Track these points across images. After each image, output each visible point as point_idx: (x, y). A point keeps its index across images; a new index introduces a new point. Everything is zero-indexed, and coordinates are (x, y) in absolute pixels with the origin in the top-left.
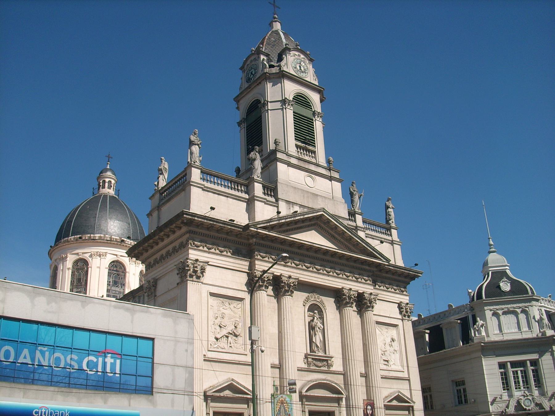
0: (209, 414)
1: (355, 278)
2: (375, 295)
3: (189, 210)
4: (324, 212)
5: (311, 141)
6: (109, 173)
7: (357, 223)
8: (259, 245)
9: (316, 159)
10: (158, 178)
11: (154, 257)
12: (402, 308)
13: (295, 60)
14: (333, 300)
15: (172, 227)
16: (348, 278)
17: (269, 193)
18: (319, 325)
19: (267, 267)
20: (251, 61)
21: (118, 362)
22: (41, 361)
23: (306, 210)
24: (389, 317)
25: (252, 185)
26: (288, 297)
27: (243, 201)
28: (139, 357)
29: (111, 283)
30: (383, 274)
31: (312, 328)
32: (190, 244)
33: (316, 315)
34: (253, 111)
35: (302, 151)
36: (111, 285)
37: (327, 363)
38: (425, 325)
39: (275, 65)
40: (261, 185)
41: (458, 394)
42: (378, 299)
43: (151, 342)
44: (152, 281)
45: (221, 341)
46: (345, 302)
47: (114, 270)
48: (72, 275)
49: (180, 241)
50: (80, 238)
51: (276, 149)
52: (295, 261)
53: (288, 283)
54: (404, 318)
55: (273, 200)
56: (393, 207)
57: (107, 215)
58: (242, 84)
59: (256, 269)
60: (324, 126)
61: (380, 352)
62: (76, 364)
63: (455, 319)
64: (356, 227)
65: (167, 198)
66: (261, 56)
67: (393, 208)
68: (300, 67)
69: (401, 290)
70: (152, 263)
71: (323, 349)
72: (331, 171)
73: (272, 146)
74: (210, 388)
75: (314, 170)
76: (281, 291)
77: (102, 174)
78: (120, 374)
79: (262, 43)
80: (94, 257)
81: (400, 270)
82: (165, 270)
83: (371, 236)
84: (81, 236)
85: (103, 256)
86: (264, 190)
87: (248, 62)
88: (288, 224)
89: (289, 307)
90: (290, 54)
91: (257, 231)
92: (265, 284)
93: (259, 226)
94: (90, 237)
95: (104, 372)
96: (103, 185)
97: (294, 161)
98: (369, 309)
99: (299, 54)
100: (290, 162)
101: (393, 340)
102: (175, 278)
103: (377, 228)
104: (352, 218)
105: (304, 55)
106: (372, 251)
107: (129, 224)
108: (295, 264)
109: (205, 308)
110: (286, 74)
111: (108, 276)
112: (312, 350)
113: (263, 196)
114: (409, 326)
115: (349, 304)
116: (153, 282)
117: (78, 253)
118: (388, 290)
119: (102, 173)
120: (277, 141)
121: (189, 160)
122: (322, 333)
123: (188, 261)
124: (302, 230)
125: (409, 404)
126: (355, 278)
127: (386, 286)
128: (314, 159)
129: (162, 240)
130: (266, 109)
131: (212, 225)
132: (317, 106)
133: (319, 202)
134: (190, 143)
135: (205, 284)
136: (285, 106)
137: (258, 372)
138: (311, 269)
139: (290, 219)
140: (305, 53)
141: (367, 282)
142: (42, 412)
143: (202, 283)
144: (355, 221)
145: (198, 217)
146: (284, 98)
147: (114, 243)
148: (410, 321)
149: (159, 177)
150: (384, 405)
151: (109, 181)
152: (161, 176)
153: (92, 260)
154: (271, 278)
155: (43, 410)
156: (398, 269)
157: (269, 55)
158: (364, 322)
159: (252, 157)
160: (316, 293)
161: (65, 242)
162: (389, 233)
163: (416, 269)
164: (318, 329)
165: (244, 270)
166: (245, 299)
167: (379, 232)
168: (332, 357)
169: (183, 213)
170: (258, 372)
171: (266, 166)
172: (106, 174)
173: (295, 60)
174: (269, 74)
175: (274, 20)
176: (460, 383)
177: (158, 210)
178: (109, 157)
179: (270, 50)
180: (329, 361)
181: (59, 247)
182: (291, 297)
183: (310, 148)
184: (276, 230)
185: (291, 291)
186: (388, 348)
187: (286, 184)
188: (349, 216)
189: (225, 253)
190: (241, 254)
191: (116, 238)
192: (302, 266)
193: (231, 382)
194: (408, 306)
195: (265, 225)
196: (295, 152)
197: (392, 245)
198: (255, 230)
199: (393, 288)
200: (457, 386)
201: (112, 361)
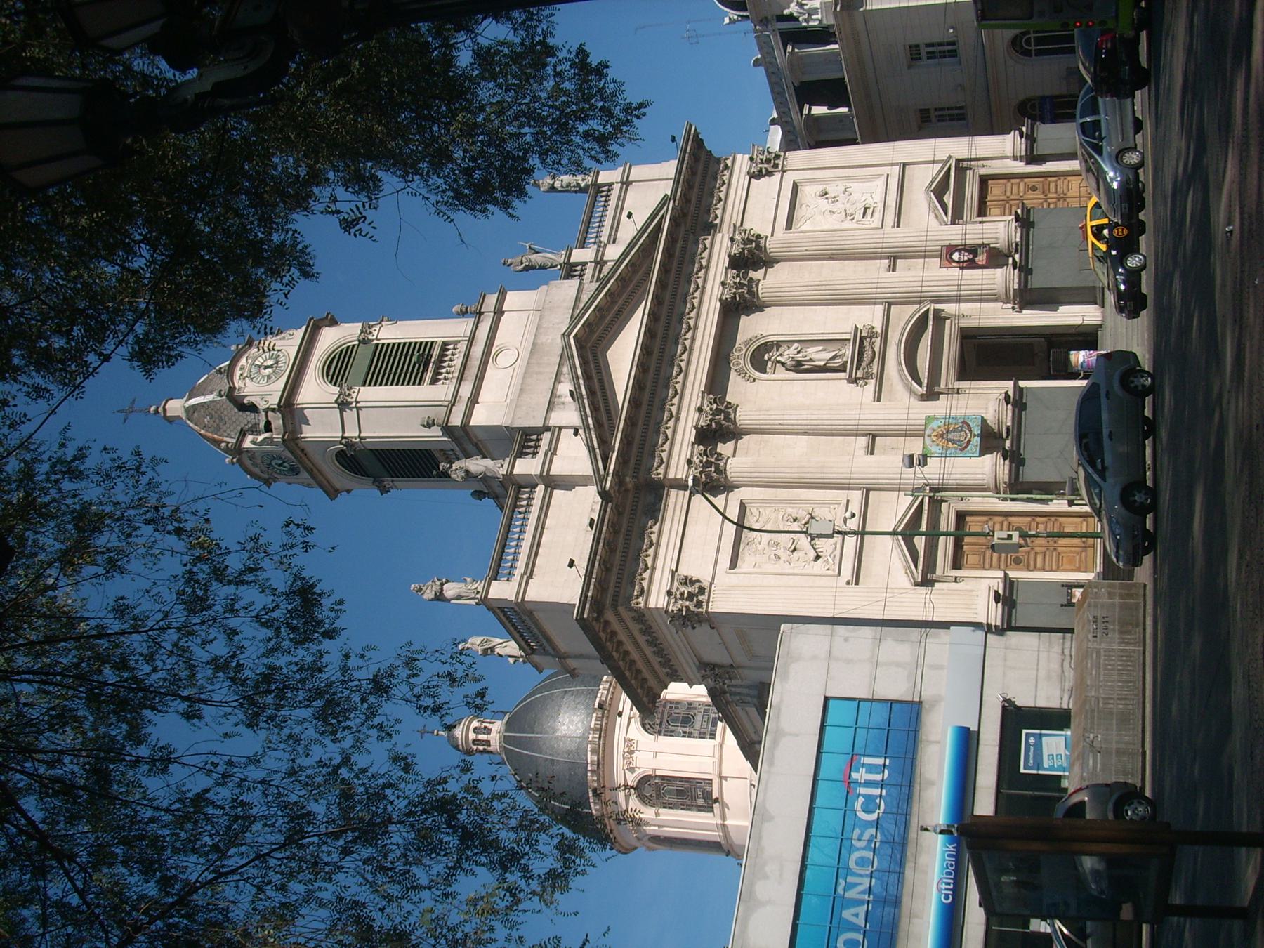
2: (734, 232)
4: (569, 335)
8: (637, 469)
9: (459, 341)
11: (657, 667)
12: (760, 171)
14: (743, 319)
17: (532, 444)
18: (792, 351)
20: (255, 465)
21: (868, 760)
23: (566, 369)
24: (778, 201)
26: (738, 414)
29: (687, 730)
31: (798, 367)
36: (692, 730)
37: (865, 338)
41: (935, 58)
49: (631, 624)
55: (546, 436)
60: (385, 318)
63: (781, 57)
65: (544, 641)
71: (839, 345)
73: (436, 433)
79: (217, 443)
86: (527, 454)
87: (256, 470)
88: (595, 409)
93: (602, 472)
94: (592, 771)
97: (466, 390)
98: (762, 245)
101: (824, 194)
102: (701, 635)
105: (241, 356)
106: (646, 235)
112: (842, 369)
113: (541, 456)
114: (796, 158)
118: (723, 198)
121: (473, 602)
124: (605, 379)
126: (699, 271)
128: (459, 345)
135: (713, 578)
139: (587, 406)
141: (708, 246)
142: (946, 889)
143: (712, 583)
144: (584, 264)
145: (588, 591)
147: (606, 724)
150: (953, 223)
152: (497, 650)
154: (701, 447)
155: (944, 886)
157: (242, 429)
162: (606, 188)
163: (681, 140)
164: (800, 355)
168: (856, 328)
169: (580, 620)
171: (476, 445)
174: (285, 433)
176: (914, 53)
177: (564, 658)
183: (436, 352)
186: (838, 207)
191: (594, 719)
197: (631, 182)
198: (609, 478)
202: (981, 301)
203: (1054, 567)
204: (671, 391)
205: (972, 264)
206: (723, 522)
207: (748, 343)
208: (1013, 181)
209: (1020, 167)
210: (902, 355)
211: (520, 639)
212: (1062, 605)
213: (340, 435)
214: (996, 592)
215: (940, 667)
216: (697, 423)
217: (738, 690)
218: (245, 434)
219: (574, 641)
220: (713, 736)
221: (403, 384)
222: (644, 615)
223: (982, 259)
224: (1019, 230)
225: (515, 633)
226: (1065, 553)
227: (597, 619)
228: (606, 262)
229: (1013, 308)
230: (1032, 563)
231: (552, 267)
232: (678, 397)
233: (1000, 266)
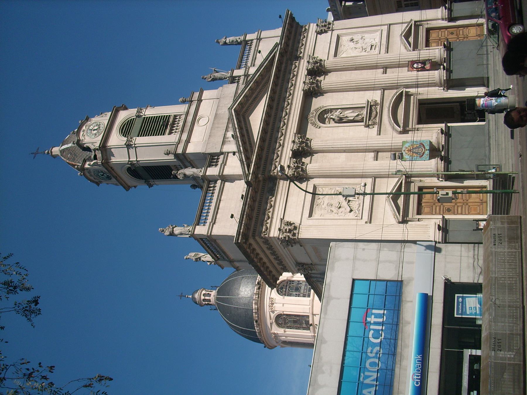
0: (419, 219)
2: (310, 58)
3: (234, 236)
5: (164, 120)
6: (196, 296)
7: (241, 75)
11: (276, 265)
13: (88, 134)
14: (314, 99)
15: (249, 252)
16: (294, 84)
17: (215, 161)
18: (337, 113)
19: (284, 164)
20: (91, 176)
21: (374, 311)
22: (373, 379)
23: (230, 125)
24: (330, 44)
25: (208, 177)
26: (312, 144)
27: (224, 186)
28: (369, 293)
29: (298, 293)
30: (289, 49)
31: (340, 120)
32: (265, 235)
33: (329, 117)
34: (138, 174)
35: (175, 128)
36: (299, 293)
37: (372, 106)
38: (337, 5)
39: (94, 154)
40: (208, 168)
42: (313, 55)
43: (356, 281)
44: (298, 267)
45: (352, 207)
46: (316, 88)
47: (286, 290)
48: (290, 328)
50: (256, 322)
51: (174, 154)
52: (279, 137)
53: (299, 144)
54: (331, 28)
55: (222, 157)
56: (224, 38)
57: (235, 298)
58: (113, 184)
60: (149, 106)
61: (364, 53)
62: (375, 348)
64: (245, 75)
65: (222, 254)
66: (86, 167)
67: (226, 38)
69: (304, 32)
71: (360, 110)
72: (192, 100)
73: (171, 157)
74: (396, 218)
75: (192, 117)
76: (307, 150)
77: (198, 302)
78: (384, 310)
79: (74, 166)
80: (274, 309)
81: (285, 33)
82: (288, 257)
83: (254, 61)
84: (255, 321)
85: (272, 301)
86: (213, 165)
87: (92, 178)
88: (244, 143)
89: (321, 142)
90: (82, 140)
91: (252, 174)
92: (300, 165)
93: (247, 172)
94: (255, 313)
95: (383, 324)
96: (208, 301)
97: (184, 137)
98: (323, 64)
99: (82, 131)
100: (186, 141)
101: (352, 40)
102: (296, 249)
103: (246, 54)
104: (236, 80)
105: (83, 125)
106: (267, 61)
107: (243, 277)
108: (281, 136)
109: (323, 222)
110: (102, 144)
111: (291, 296)
112: (361, 121)
113: (219, 166)
115: (318, 84)
116: (299, 267)
117: (270, 323)
118: (304, 44)
119: (197, 302)
120: (166, 153)
122: (345, 110)
123: (280, 238)
125: (413, 25)
127: (300, 46)
128: (182, 116)
129: (261, 259)
130: (136, 162)
131: (247, 216)
132: (131, 113)
133: (223, 112)
135: (301, 222)
136: (133, 144)
137: (381, 173)
138: (286, 121)
140: (80, 126)
141: (297, 66)
142: (417, 379)
143: (300, 224)
144: (239, 77)
145: (240, 229)
146: (125, 146)
147: (261, 291)
148: (334, 22)
149: (202, 260)
150: (414, 50)
151: (203, 296)
152: (202, 259)
153: (276, 311)
154: (295, 159)
155: (415, 377)
156: (285, 34)
157: (84, 159)
158: (335, 69)
159: (183, 177)
160: (308, 116)
161: (261, 336)
162: (250, 42)
163: (284, 17)
164: (342, 115)
165: (288, 185)
166: (314, 184)
167: (249, 52)
168: (368, 101)
169: (237, 243)
170: (381, 173)
171: (190, 162)
172: (197, 298)
173: (88, 134)
174: (103, 160)
175: (50, 154)
177: (233, 262)
178: (181, 296)
179: (80, 159)
180: (371, 104)
181: (265, 340)
182: (312, 141)
183: (171, 120)
185: (306, 140)
186: (359, 46)
187: (207, 145)
188: (234, 83)
189: (272, 203)
190: (273, 188)
191: (256, 289)
192: (283, 130)
193: (390, 199)
194: (319, 24)
195: (246, 166)
196: (175, 135)
197: (261, 39)
198: (250, 175)
199: (302, 39)
201: (373, 316)
202: (428, 86)
203: (467, 213)
204: (280, 133)
205: (423, 69)
206: (305, 195)
207: (317, 110)
208: (442, 30)
209: (445, 23)
210: (390, 113)
211: (212, 253)
212: (474, 230)
213: (128, 160)
214: (439, 225)
215: (412, 263)
216: (293, 148)
217: (315, 276)
218: (86, 161)
219: (235, 254)
220: (309, 296)
221: (156, 135)
222: (268, 241)
223: (428, 66)
224: (445, 52)
225: (209, 250)
226: (472, 206)
227: (245, 243)
228: (249, 75)
229: (444, 89)
230: (456, 211)
231: (225, 78)
232: (283, 136)
233: (437, 70)
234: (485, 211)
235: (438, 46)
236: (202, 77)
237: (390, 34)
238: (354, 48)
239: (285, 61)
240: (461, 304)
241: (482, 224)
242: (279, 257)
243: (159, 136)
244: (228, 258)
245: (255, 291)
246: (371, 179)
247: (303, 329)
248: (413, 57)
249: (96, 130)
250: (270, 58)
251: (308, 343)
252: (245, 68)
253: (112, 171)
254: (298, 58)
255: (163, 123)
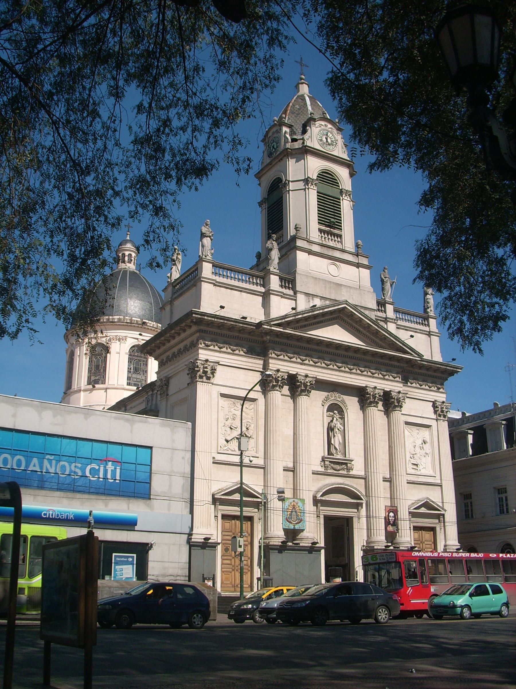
1: (382, 375)
2: (404, 394)
3: (200, 309)
4: (346, 304)
5: (336, 223)
6: (129, 246)
8: (274, 342)
9: (342, 244)
10: (171, 269)
12: (437, 407)
17: (287, 285)
18: (339, 425)
20: (273, 133)
21: (118, 471)
23: (328, 303)
24: (421, 417)
27: (258, 295)
29: (132, 370)
31: (330, 429)
35: (326, 236)
36: (132, 372)
37: (347, 466)
39: (299, 138)
40: (278, 277)
41: (500, 502)
43: (150, 450)
47: (136, 356)
48: (89, 361)
49: (190, 339)
55: (291, 292)
59: (270, 368)
60: (354, 203)
61: (408, 455)
63: (500, 418)
65: (180, 292)
67: (432, 294)
68: (327, 139)
70: (165, 360)
71: (343, 451)
79: (285, 112)
86: (281, 282)
88: (306, 319)
89: (305, 408)
90: (315, 125)
92: (279, 384)
93: (272, 323)
94: (109, 319)
97: (316, 248)
98: (397, 409)
99: (326, 123)
102: (185, 378)
106: (401, 345)
112: (330, 453)
113: (280, 290)
114: (444, 426)
118: (422, 387)
122: (342, 434)
125: (439, 512)
128: (340, 244)
134: (201, 235)
139: (308, 314)
140: (332, 121)
141: (396, 379)
142: (49, 514)
143: (212, 384)
144: (385, 312)
145: (208, 316)
147: (135, 326)
150: (410, 513)
151: (129, 254)
152: (174, 267)
154: (286, 377)
155: (51, 513)
157: (292, 126)
162: (426, 323)
163: (453, 364)
164: (337, 430)
168: (352, 461)
169: (191, 313)
171: (286, 254)
174: (291, 150)
176: (502, 491)
177: (170, 304)
179: (293, 120)
182: (307, 397)
183: (336, 231)
184: (292, 326)
185: (308, 390)
186: (418, 450)
191: (137, 319)
194: (445, 404)
195: (280, 321)
197: (430, 337)
198: (269, 327)
200: (499, 494)
202: (368, 529)
203: (223, 570)
205: (387, 522)
206: (247, 389)
207: (343, 402)
208: (433, 545)
210: (337, 486)
211: (180, 279)
213: (290, 180)
214: (210, 539)
215: (169, 509)
216: (299, 375)
218: (290, 127)
219: (179, 312)
220: (129, 384)
221: (318, 213)
223: (390, 528)
226: (231, 576)
229: (364, 546)
230: (226, 558)
231: (383, 294)
233: (386, 539)
234: (225, 589)
235: (414, 541)
236: (386, 267)
237: (430, 486)
238: (414, 444)
239: (402, 365)
240: (126, 560)
241: (210, 583)
242: (176, 358)
243: (317, 218)
244: (175, 298)
245: (135, 319)
246: (263, 464)
247: (88, 377)
248: (402, 513)
249: (327, 141)
250: (405, 348)
251: (71, 383)
252: (395, 318)
253: (277, 160)
254: (405, 380)
255: (333, 222)
